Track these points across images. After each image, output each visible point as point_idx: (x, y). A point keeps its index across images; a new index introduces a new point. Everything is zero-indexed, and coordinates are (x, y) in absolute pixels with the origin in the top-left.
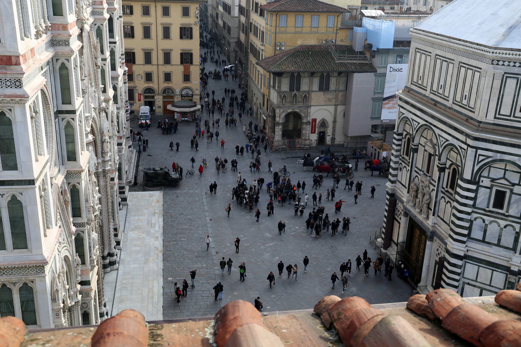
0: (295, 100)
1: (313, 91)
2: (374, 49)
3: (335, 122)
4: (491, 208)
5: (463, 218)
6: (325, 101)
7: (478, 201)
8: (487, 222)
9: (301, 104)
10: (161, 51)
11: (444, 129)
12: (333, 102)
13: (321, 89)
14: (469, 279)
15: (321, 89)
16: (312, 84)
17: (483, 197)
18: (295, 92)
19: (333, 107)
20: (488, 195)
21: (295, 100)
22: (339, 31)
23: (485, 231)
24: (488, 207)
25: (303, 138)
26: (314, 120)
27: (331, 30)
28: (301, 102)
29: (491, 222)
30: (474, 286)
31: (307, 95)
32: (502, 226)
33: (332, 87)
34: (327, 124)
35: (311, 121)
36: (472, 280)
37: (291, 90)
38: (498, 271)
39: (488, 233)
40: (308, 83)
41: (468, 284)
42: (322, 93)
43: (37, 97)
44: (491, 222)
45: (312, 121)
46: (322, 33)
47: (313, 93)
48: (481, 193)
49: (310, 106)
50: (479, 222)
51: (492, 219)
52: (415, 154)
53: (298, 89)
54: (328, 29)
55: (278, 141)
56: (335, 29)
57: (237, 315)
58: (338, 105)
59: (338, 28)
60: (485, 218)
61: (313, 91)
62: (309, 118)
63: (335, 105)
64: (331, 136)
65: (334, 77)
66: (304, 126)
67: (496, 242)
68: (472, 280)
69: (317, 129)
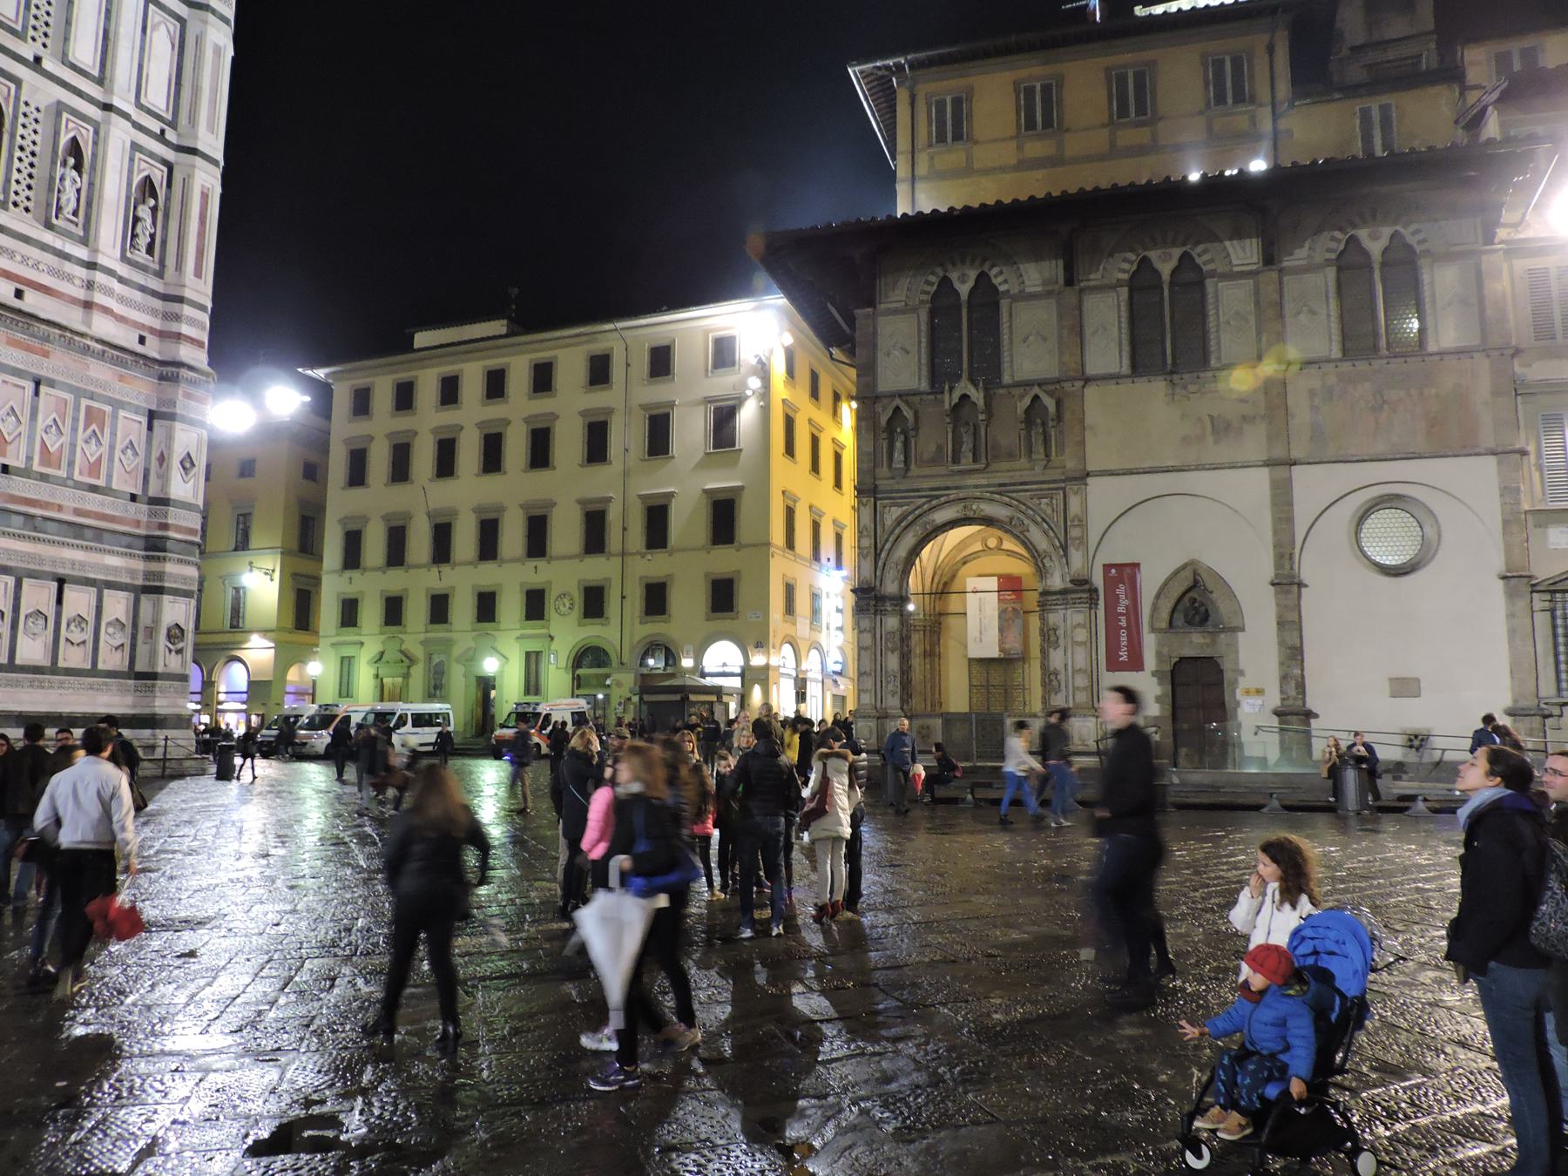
0: (967, 447)
9: (1021, 470)
10: (425, 518)
11: (485, 335)
13: (1145, 358)
15: (1145, 358)
16: (1079, 331)
18: (964, 387)
19: (1260, 479)
21: (967, 447)
26: (1124, 574)
28: (1011, 456)
35: (1098, 580)
37: (939, 376)
43: (894, 159)
45: (1111, 583)
47: (1091, 392)
49: (1083, 477)
53: (988, 368)
55: (840, 772)
57: (199, 392)
62: (1076, 558)
64: (1274, 699)
69: (1150, 643)
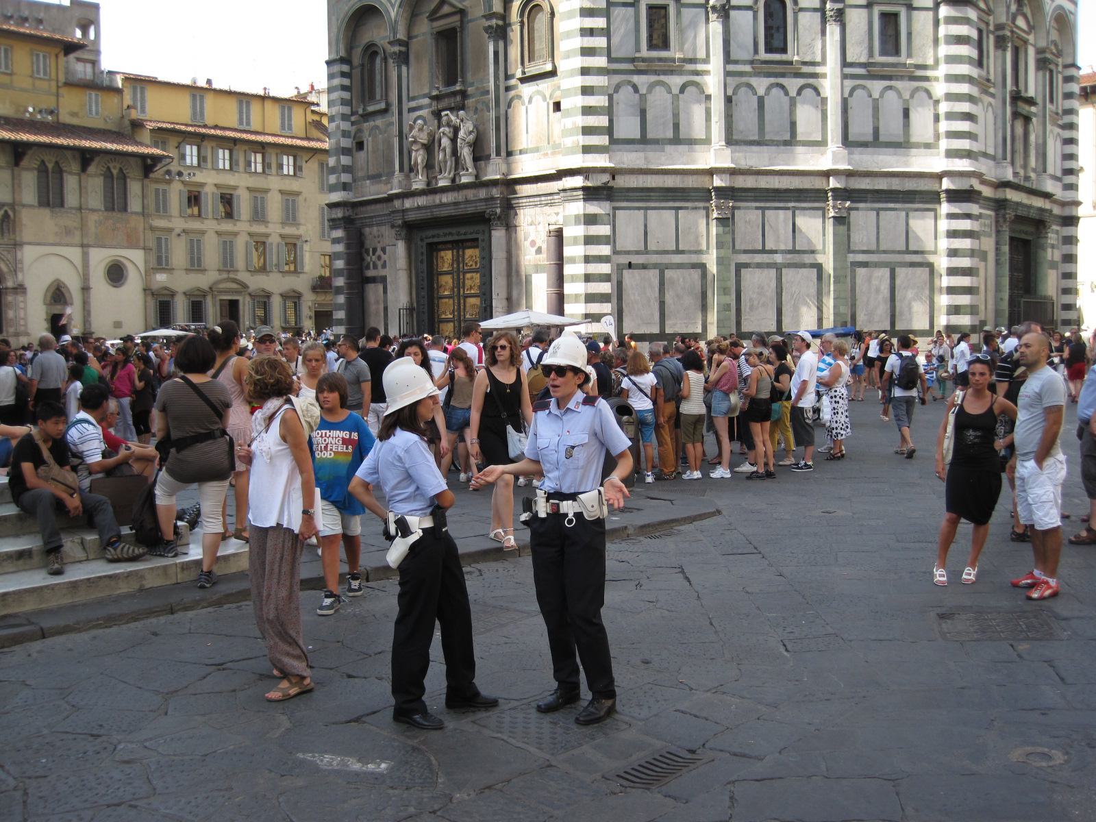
1: (24, 206)
2: (72, 363)
3: (86, 289)
4: (645, 52)
5: (592, 87)
6: (56, 234)
7: (615, 40)
8: (643, 91)
12: (77, 238)
14: (628, 253)
17: (622, 31)
20: (632, 21)
22: (62, 91)
23: (643, 113)
24: (638, 50)
25: (12, 330)
27: (45, 85)
29: (651, 86)
30: (644, 267)
31: (11, 213)
32: (676, 91)
33: (71, 199)
34: (67, 295)
36: (637, 253)
38: (686, 208)
39: (649, 116)
40: (9, 181)
41: (630, 265)
42: (46, 212)
44: (651, 86)
46: (23, 90)
48: (619, 19)
49: (21, 244)
50: (625, 94)
51: (653, 78)
52: (404, 68)
54: (38, 83)
56: (54, 84)
58: (89, 246)
59: (60, 84)
60: (636, 79)
61: (24, 206)
63: (82, 246)
65: (71, 173)
66: (10, 298)
67: (670, 134)
68: (637, 253)
